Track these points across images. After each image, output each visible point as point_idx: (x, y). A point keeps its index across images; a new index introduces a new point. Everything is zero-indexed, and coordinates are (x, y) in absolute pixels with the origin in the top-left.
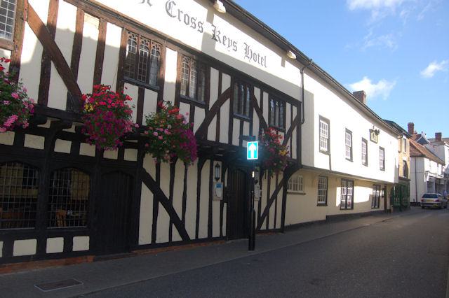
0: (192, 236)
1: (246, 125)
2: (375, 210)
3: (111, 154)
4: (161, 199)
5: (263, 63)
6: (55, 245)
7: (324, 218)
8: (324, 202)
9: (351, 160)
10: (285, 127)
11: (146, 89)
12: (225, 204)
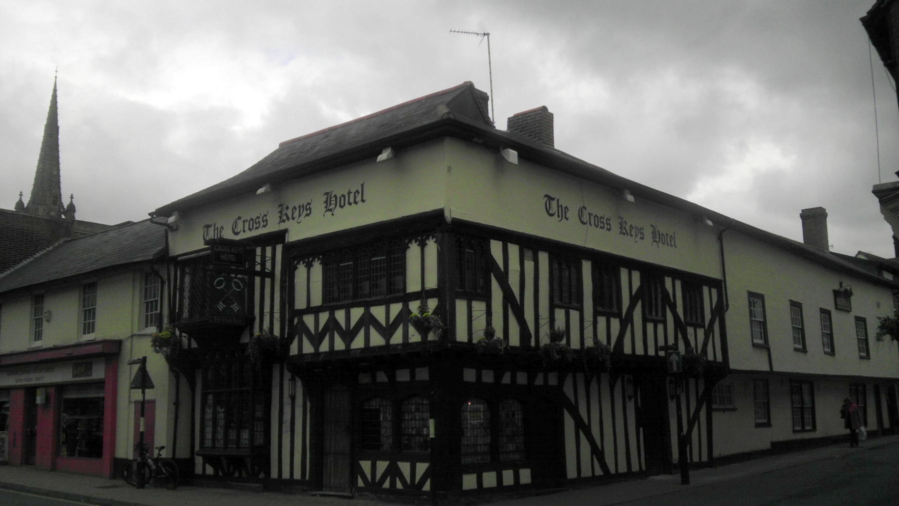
0: (612, 471)
1: (660, 327)
2: (799, 436)
3: (539, 381)
4: (582, 427)
5: (673, 243)
6: (508, 477)
7: (766, 445)
8: (765, 421)
9: (804, 350)
10: (703, 320)
11: (570, 310)
12: (641, 429)
